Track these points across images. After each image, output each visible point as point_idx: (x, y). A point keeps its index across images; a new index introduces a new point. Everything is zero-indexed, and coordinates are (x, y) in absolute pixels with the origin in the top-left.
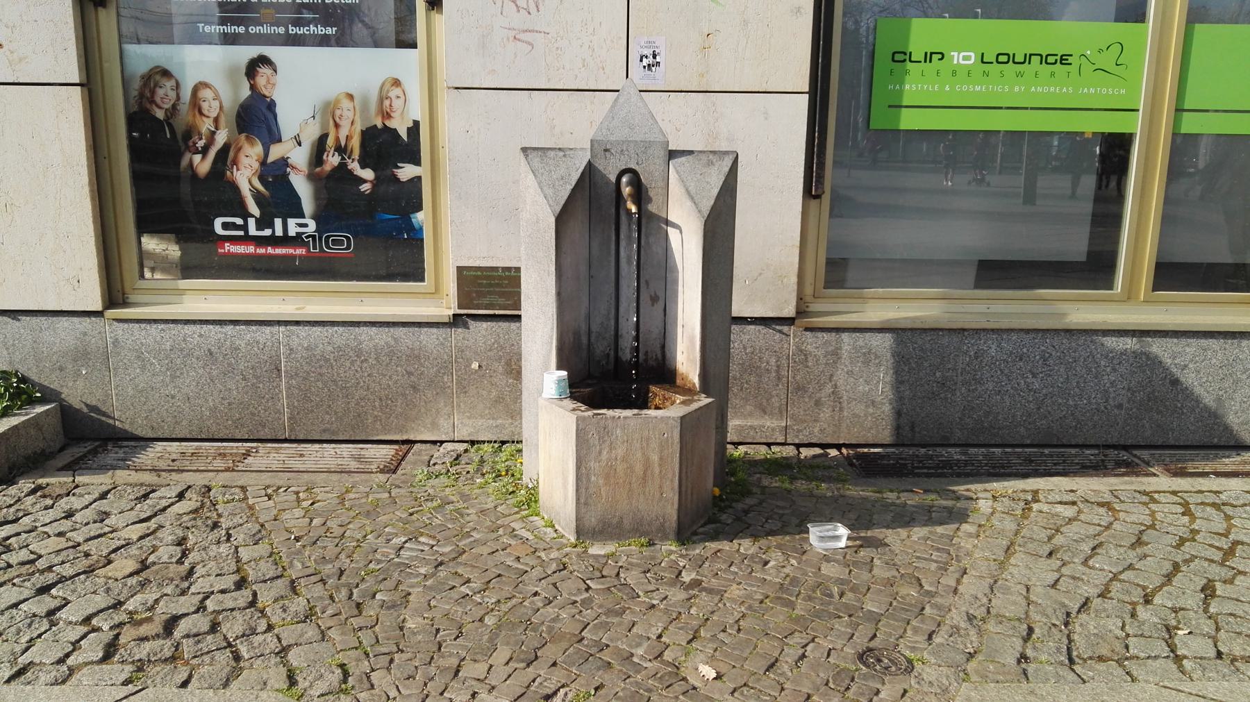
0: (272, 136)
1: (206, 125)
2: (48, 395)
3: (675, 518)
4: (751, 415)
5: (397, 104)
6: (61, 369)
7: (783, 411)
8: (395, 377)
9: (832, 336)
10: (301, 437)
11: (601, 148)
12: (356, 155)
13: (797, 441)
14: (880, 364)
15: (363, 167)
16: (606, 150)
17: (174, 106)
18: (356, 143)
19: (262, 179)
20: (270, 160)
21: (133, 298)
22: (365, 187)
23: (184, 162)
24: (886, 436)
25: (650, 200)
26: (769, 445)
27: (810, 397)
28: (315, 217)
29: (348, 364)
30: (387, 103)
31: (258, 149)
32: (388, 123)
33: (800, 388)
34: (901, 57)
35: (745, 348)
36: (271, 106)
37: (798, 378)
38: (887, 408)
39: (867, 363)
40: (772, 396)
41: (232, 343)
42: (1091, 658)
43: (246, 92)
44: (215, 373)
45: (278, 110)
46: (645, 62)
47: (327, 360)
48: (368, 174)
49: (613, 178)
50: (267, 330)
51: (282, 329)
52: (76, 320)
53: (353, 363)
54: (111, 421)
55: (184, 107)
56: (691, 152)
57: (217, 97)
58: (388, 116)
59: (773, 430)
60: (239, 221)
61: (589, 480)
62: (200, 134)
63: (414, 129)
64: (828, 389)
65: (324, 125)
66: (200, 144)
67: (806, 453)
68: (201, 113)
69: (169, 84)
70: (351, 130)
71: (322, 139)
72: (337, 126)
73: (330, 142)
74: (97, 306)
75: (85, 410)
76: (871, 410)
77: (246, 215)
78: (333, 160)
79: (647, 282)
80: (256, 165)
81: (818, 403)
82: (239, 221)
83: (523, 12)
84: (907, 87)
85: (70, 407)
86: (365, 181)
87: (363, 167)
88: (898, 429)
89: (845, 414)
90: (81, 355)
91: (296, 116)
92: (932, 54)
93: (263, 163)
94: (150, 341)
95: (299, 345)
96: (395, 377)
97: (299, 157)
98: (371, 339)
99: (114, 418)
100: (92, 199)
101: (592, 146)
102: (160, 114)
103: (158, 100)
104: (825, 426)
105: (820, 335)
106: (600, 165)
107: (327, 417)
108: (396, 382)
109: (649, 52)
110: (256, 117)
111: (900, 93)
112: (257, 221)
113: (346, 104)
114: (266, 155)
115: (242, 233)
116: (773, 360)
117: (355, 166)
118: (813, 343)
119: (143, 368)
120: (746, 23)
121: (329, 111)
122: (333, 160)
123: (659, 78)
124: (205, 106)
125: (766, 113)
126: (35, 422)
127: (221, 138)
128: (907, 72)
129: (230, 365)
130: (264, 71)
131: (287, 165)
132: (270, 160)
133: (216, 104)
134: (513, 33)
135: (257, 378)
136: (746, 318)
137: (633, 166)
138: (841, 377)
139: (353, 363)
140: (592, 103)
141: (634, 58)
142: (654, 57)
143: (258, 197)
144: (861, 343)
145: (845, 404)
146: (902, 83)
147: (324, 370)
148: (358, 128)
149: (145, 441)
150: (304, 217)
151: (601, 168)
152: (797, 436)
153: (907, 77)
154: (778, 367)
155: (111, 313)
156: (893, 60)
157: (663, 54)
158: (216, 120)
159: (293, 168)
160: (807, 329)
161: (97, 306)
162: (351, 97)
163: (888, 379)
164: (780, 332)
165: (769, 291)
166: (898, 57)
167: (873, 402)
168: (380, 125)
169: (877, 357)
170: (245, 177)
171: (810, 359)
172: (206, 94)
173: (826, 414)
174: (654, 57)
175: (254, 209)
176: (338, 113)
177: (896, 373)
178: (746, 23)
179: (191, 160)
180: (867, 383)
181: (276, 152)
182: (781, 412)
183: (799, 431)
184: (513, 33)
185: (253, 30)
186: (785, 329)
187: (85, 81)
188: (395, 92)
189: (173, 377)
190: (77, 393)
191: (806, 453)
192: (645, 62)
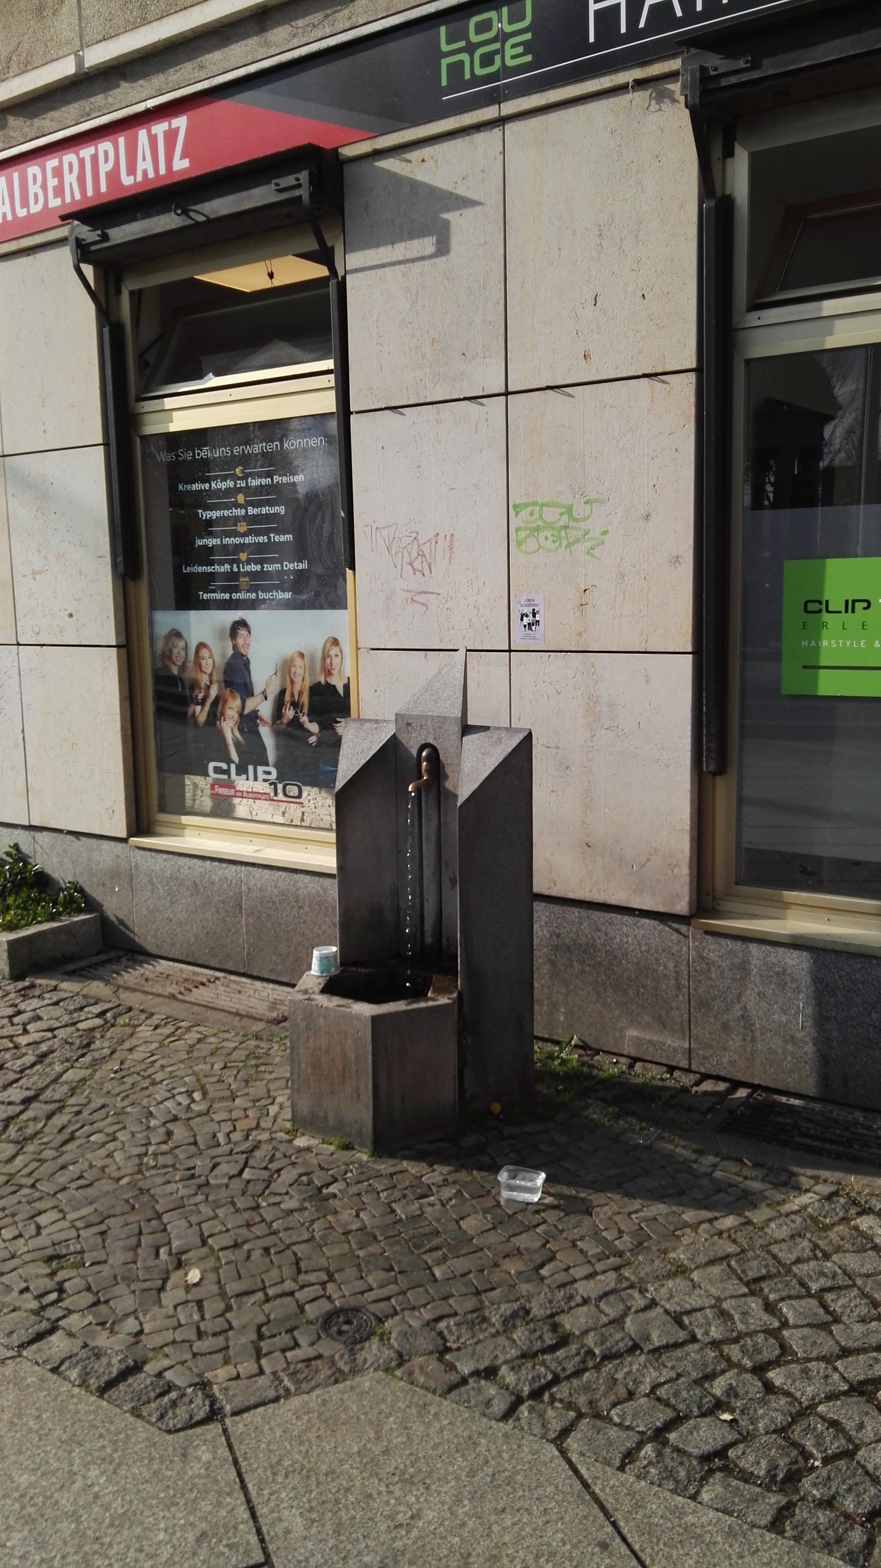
0: (247, 691)
1: (204, 680)
2: (91, 905)
3: (370, 1124)
4: (648, 1027)
5: (336, 661)
6: (104, 885)
7: (687, 1028)
8: (323, 927)
9: (738, 945)
10: (255, 974)
11: (404, 721)
12: (306, 711)
13: (703, 1070)
14: (798, 990)
15: (310, 721)
16: (408, 724)
17: (184, 663)
18: (305, 699)
19: (241, 730)
20: (246, 712)
21: (159, 829)
22: (313, 739)
23: (191, 710)
24: (809, 1084)
25: (446, 777)
26: (671, 1069)
27: (716, 1017)
28: (276, 766)
29: (288, 909)
30: (328, 661)
31: (238, 702)
32: (329, 680)
33: (704, 1004)
34: (815, 607)
35: (639, 945)
36: (247, 664)
37: (700, 991)
38: (809, 1048)
39: (782, 986)
40: (671, 1009)
41: (210, 878)
42: (561, 1401)
43: (230, 652)
44: (198, 903)
45: (252, 667)
46: (526, 621)
47: (274, 903)
48: (314, 727)
49: (414, 752)
50: (233, 868)
51: (243, 868)
52: (113, 843)
53: (292, 908)
54: (132, 935)
55: (190, 664)
56: (486, 728)
57: (211, 656)
58: (328, 673)
59: (675, 1050)
60: (224, 766)
61: (300, 1066)
62: (200, 688)
63: (347, 687)
64: (737, 1011)
65: (283, 679)
66: (201, 696)
67: (708, 1086)
68: (201, 671)
69: (181, 644)
70: (302, 684)
71: (283, 692)
72: (292, 682)
73: (287, 697)
74: (123, 834)
75: (117, 923)
76: (790, 1048)
77: (229, 761)
78: (289, 713)
79: (446, 863)
80: (236, 716)
81: (726, 1027)
82: (224, 766)
83: (419, 574)
84: (825, 643)
85: (107, 917)
86: (312, 734)
87: (310, 721)
88: (824, 1079)
89: (759, 1046)
90: (115, 874)
91: (263, 675)
92: (854, 601)
93: (241, 715)
94: (157, 868)
95: (255, 885)
96: (323, 927)
97: (266, 710)
98: (306, 887)
99: (133, 932)
100: (124, 742)
101: (396, 720)
102: (175, 671)
103: (174, 658)
104: (736, 1057)
105: (723, 941)
106: (403, 738)
107: (274, 958)
108: (324, 932)
109: (528, 610)
110: (237, 675)
111: (817, 650)
112: (237, 766)
113: (298, 662)
114: (243, 707)
115: (226, 777)
116: (671, 965)
117: (304, 719)
118: (714, 949)
119: (152, 891)
120: (622, 576)
121: (286, 668)
122: (289, 713)
123: (543, 637)
124: (203, 662)
125: (647, 676)
126: (68, 930)
127: (214, 692)
128: (824, 625)
129: (208, 897)
130: (242, 632)
131: (257, 717)
132: (246, 712)
133: (210, 662)
134: (410, 595)
135: (226, 912)
136: (634, 910)
137: (431, 741)
138: (750, 998)
139: (292, 908)
140: (479, 663)
141: (516, 617)
142: (534, 616)
143: (237, 744)
144: (772, 959)
145: (758, 1034)
146: (818, 638)
147: (272, 912)
148: (308, 684)
149: (149, 956)
150: (267, 765)
151: (404, 741)
152: (703, 1064)
153: (824, 632)
154: (677, 973)
155: (133, 840)
156: (806, 611)
157: (541, 612)
158: (211, 675)
159: (262, 720)
160: (707, 933)
161: (123, 834)
162: (302, 655)
163: (809, 1011)
164: (678, 931)
165: (658, 881)
166: (811, 607)
167: (792, 1038)
168: (323, 681)
169: (794, 980)
170: (229, 728)
171: (713, 969)
172: (204, 653)
173: (735, 1042)
174: (534, 616)
175: (235, 756)
176: (293, 670)
177: (819, 1004)
178: (622, 576)
179: (194, 712)
180: (784, 1011)
181: (251, 704)
182: (683, 1031)
183: (705, 1058)
184: (410, 595)
185: (235, 596)
186: (683, 928)
187: (124, 643)
188: (334, 651)
189: (171, 902)
190: (114, 906)
191: (708, 1086)
192: (526, 621)
